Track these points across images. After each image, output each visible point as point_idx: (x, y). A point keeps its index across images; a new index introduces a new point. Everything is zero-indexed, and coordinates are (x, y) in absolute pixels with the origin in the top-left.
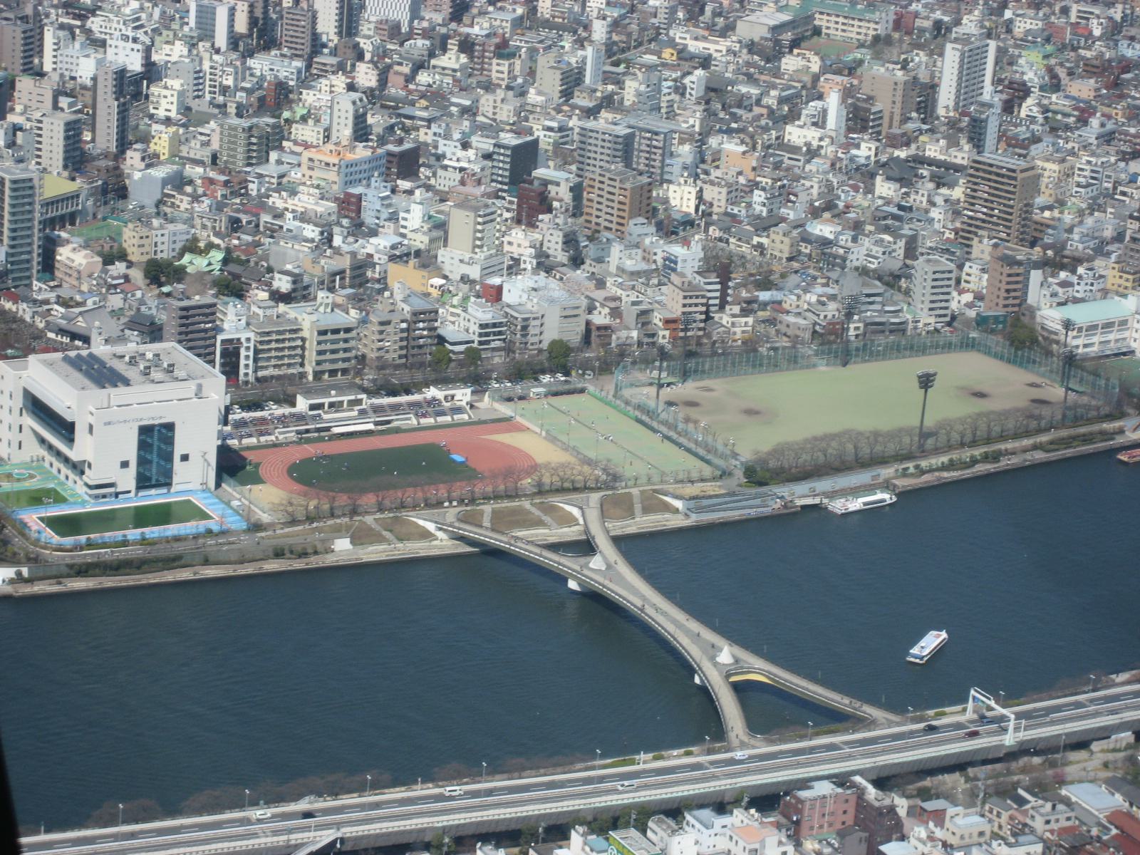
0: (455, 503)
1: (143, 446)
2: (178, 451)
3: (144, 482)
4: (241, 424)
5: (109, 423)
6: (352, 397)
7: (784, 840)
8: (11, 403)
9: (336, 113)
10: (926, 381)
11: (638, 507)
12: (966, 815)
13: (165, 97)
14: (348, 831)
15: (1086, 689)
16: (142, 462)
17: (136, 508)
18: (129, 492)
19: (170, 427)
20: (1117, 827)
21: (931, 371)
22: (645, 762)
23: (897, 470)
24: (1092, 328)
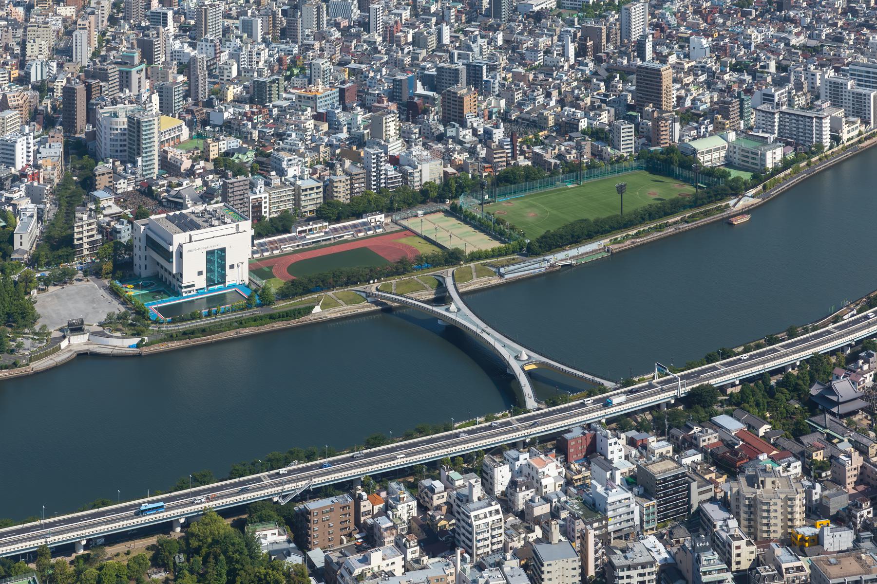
0: (376, 281)
1: (209, 261)
2: (228, 264)
3: (210, 282)
4: (259, 245)
5: (190, 251)
6: (321, 225)
7: (559, 465)
8: (140, 244)
9: (313, 70)
10: (621, 189)
11: (474, 274)
12: (658, 441)
13: (227, 69)
14: (316, 480)
15: (498, 415)
16: (209, 270)
17: (207, 297)
18: (203, 288)
19: (223, 250)
20: (743, 440)
21: (623, 184)
22: (480, 423)
23: (610, 241)
24: (709, 152)
